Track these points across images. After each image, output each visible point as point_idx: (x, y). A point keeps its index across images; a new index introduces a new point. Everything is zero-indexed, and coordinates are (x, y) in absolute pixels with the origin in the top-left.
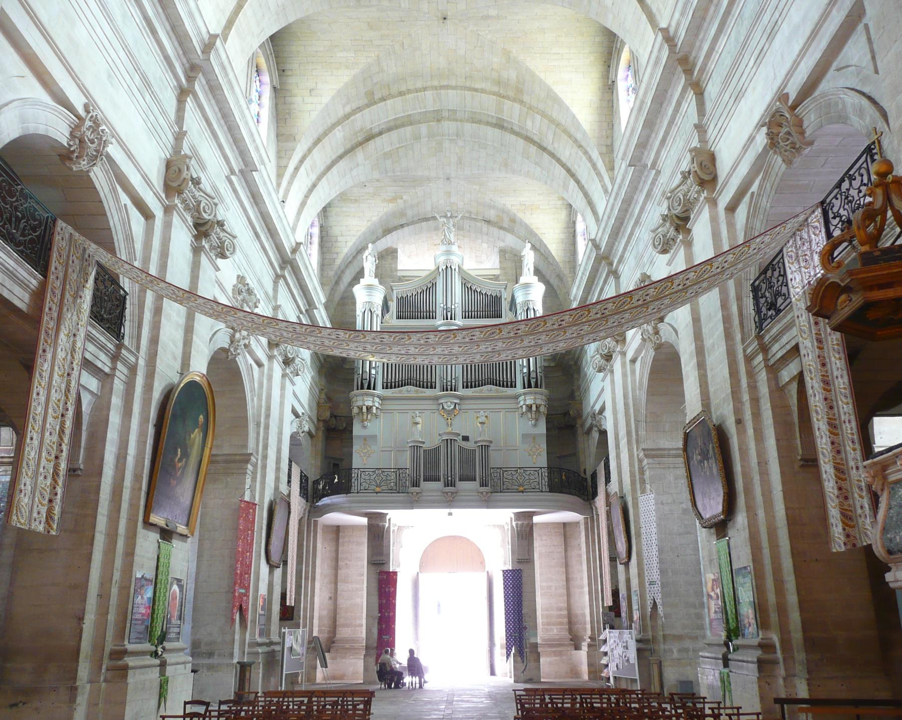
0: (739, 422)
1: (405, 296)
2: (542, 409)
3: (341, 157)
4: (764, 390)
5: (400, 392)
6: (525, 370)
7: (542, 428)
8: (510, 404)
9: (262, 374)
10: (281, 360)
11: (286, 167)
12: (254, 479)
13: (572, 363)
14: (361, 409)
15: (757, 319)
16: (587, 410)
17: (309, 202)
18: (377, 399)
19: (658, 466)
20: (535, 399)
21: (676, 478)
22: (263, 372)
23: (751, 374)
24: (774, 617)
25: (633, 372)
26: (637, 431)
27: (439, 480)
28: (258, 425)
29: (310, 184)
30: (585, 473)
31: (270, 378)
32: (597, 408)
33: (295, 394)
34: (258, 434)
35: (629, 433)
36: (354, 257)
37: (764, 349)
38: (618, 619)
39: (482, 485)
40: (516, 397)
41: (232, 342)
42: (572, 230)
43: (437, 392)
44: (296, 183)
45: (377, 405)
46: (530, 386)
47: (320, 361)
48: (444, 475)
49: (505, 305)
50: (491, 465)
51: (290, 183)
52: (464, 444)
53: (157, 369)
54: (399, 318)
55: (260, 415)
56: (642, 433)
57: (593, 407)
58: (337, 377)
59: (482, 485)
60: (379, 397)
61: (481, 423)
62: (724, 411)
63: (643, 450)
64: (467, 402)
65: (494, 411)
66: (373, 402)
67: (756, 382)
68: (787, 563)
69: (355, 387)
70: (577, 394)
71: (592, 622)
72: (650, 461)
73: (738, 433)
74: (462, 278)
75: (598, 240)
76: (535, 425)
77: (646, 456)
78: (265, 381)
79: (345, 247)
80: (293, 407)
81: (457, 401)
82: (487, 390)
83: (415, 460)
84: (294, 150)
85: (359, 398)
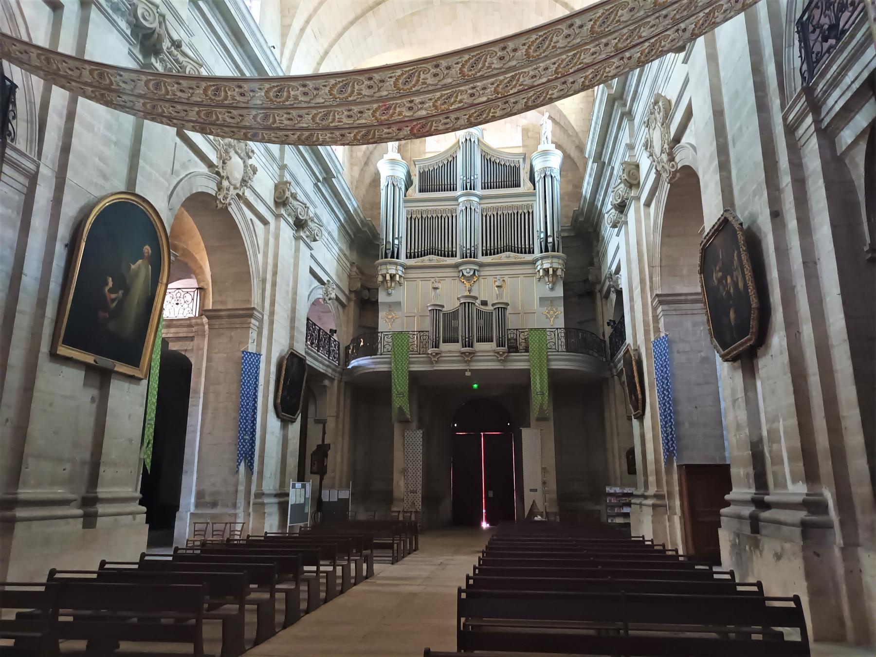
0: (776, 215)
1: (426, 170)
3: (352, 23)
4: (813, 163)
5: (422, 261)
6: (542, 235)
7: (559, 292)
8: (527, 269)
9: (267, 232)
10: (292, 223)
11: (290, 26)
12: (260, 334)
13: (590, 230)
14: (384, 276)
15: (805, 67)
16: (605, 272)
20: (552, 263)
21: (695, 325)
23: (794, 149)
24: (825, 466)
25: (647, 216)
27: (458, 342)
28: (264, 281)
29: (322, 52)
30: (604, 336)
31: (277, 237)
32: (614, 268)
33: (312, 256)
34: (264, 290)
35: (642, 281)
37: (815, 106)
38: (632, 476)
39: (498, 345)
40: (533, 263)
41: (219, 189)
43: (457, 260)
44: (302, 46)
46: (547, 250)
49: (524, 175)
51: (296, 44)
52: (483, 308)
53: (67, 180)
54: (420, 191)
55: (265, 272)
56: (657, 279)
57: (610, 268)
58: (364, 242)
59: (498, 345)
60: (402, 265)
61: (498, 287)
62: (754, 207)
63: (657, 295)
64: (487, 268)
65: (512, 276)
67: (800, 158)
68: (847, 391)
70: (595, 260)
72: (666, 307)
73: (774, 230)
74: (482, 151)
76: (552, 289)
77: (661, 303)
78: (272, 241)
81: (476, 268)
82: (504, 257)
84: (297, 8)
85: (383, 267)
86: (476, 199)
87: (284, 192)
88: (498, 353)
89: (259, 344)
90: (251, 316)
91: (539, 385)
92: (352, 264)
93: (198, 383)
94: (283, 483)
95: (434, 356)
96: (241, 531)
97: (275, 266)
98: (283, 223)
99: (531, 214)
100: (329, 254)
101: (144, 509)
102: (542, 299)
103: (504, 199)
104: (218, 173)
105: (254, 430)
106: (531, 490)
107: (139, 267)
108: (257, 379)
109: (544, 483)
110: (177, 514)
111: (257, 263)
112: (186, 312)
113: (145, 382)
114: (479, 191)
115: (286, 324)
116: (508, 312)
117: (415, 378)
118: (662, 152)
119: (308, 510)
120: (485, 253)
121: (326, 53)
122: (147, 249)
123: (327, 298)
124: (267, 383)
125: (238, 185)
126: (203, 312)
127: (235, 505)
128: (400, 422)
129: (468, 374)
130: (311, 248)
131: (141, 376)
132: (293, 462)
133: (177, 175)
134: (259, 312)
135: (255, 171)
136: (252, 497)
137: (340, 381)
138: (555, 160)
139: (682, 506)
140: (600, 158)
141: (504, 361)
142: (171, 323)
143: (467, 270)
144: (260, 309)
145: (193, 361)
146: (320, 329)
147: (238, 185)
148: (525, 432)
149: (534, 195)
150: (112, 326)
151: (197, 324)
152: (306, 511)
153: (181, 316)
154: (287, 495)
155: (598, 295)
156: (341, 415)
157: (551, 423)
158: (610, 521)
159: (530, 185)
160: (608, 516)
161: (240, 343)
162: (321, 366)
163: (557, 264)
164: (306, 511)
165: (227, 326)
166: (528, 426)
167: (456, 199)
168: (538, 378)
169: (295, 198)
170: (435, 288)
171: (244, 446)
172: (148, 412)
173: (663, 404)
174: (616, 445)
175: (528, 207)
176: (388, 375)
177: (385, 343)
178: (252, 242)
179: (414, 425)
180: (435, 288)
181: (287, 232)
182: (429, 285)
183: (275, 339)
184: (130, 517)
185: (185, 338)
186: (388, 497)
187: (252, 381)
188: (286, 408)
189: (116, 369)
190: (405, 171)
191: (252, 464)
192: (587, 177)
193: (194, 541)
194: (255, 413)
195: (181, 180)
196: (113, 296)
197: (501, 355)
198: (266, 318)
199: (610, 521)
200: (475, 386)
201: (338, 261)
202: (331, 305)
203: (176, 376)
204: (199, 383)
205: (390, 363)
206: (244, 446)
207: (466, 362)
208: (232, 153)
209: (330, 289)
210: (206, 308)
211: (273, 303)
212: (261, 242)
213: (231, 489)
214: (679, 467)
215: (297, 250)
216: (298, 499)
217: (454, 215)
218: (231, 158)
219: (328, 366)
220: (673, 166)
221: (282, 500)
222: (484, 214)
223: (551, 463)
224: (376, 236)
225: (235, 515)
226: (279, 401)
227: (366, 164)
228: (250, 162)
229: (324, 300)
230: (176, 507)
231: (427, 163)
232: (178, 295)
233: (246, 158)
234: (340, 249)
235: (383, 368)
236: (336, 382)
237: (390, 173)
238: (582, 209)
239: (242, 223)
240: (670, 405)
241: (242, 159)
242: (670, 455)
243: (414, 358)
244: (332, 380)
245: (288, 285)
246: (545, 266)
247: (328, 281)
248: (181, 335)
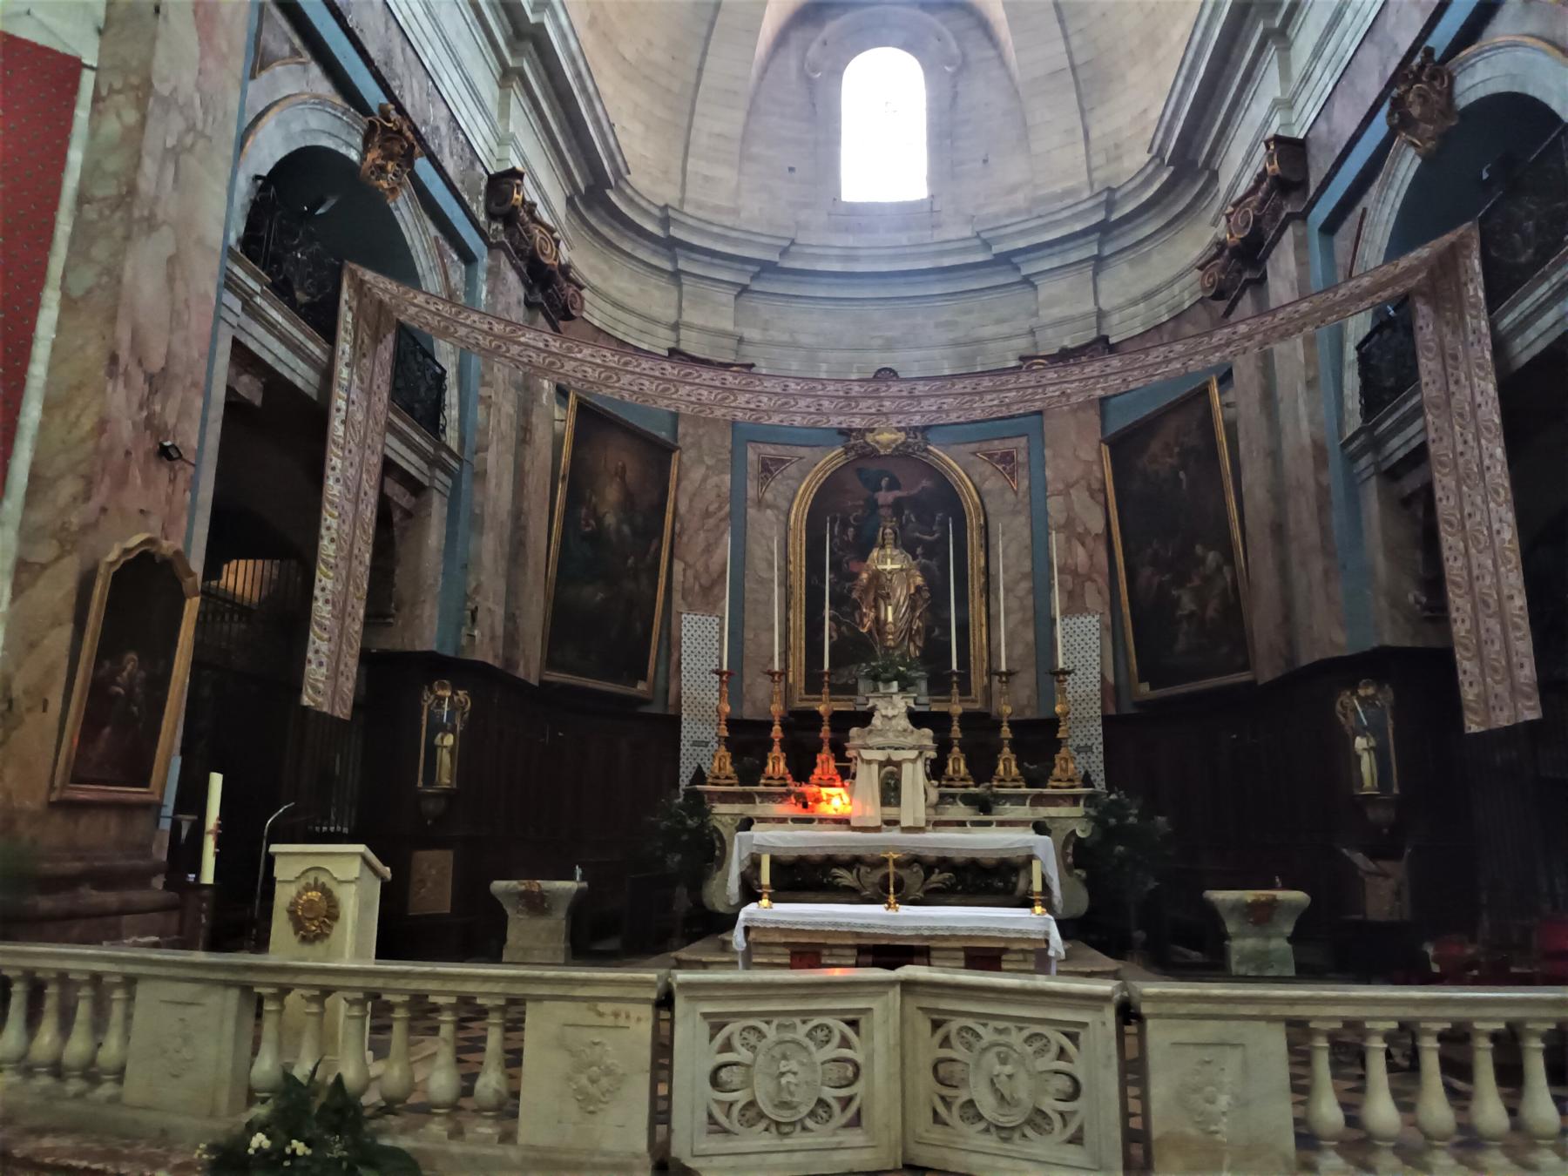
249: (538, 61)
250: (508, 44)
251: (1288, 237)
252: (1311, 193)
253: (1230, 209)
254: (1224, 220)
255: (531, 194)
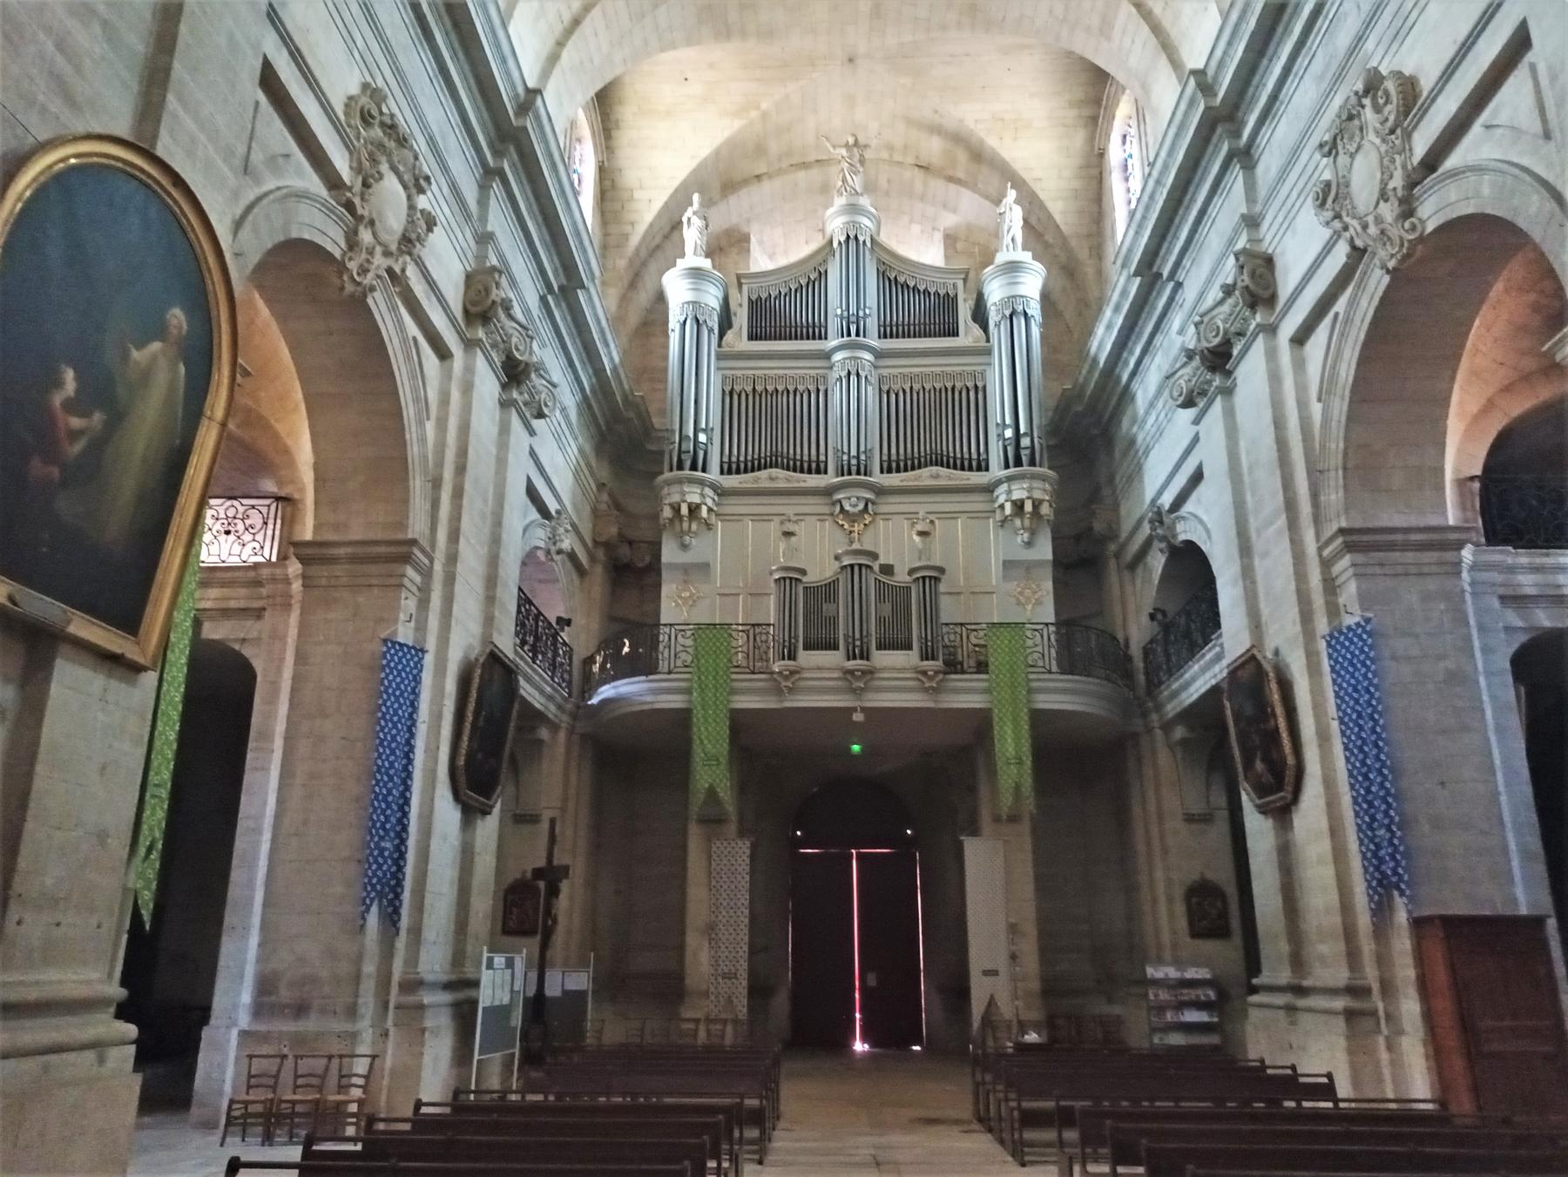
2: (1045, 510)
6: (1009, 433)
8: (976, 503)
9: (447, 376)
12: (424, 603)
14: (676, 509)
17: (565, 54)
18: (708, 491)
19: (1378, 570)
20: (1030, 490)
21: (1426, 597)
22: (451, 369)
25: (1299, 365)
26: (1315, 496)
28: (437, 483)
29: (567, 17)
31: (468, 388)
33: (533, 453)
36: (666, 237)
40: (989, 489)
42: (1095, 172)
45: (710, 502)
46: (1018, 463)
47: (598, 426)
48: (846, 636)
49: (964, 311)
50: (944, 619)
54: (751, 337)
55: (440, 464)
56: (1333, 497)
58: (628, 442)
60: (714, 487)
61: (921, 534)
66: (703, 495)
69: (666, 466)
71: (21, 983)
72: (1360, 558)
74: (879, 261)
75: (1211, 72)
77: (1350, 547)
78: (455, 395)
79: (646, 207)
80: (529, 480)
82: (926, 476)
83: (787, 607)
85: (675, 488)
86: (868, 356)
87: (487, 291)
88: (924, 673)
89: (421, 628)
90: (406, 559)
91: (1012, 745)
92: (601, 486)
93: (270, 716)
94: (458, 958)
95: (786, 678)
96: (367, 1077)
97: (462, 453)
98: (480, 362)
99: (981, 390)
100: (557, 454)
101: (132, 1030)
102: (1008, 565)
103: (927, 363)
104: (349, 206)
105: (405, 829)
106: (986, 973)
107: (154, 358)
108: (414, 707)
109: (1013, 957)
110: (206, 1033)
111: (423, 440)
112: (248, 550)
113: (150, 678)
114: (874, 342)
115: (478, 585)
116: (942, 588)
117: (740, 723)
118: (1383, 196)
119: (517, 1019)
120: (887, 469)
121: (576, 22)
122: (177, 317)
123: (553, 549)
124: (437, 717)
125: (393, 247)
126: (291, 546)
127: (352, 1012)
128: (704, 821)
129: (858, 717)
130: (532, 433)
131: (141, 660)
132: (483, 905)
133: (258, 181)
134: (423, 551)
135: (431, 223)
136: (394, 990)
137: (571, 731)
138: (1032, 283)
139: (1428, 1016)
140: (1151, 265)
141: (936, 691)
142: (216, 576)
143: (851, 500)
144: (425, 543)
145: (258, 665)
146: (540, 613)
147: (393, 247)
148: (974, 849)
149: (989, 352)
150: (66, 506)
151: (274, 580)
152: (513, 1023)
153: (234, 561)
154: (475, 984)
155: (1112, 563)
156: (571, 805)
157: (1025, 827)
158: (1156, 1041)
159: (976, 330)
160: (1154, 1030)
161: (380, 621)
162: (537, 694)
163: (1042, 491)
164: (513, 1023)
165: (344, 580)
166: (975, 832)
167: (827, 356)
168: (1008, 729)
169: (507, 308)
170: (788, 534)
171: (380, 866)
172: (155, 764)
173: (1361, 775)
174: (1159, 874)
175: (973, 375)
176: (682, 719)
177: (675, 647)
178: (415, 390)
179: (732, 828)
180: (788, 534)
181: (487, 384)
182: (774, 527)
183: (457, 627)
184: (90, 1055)
185: (243, 612)
186: (669, 988)
187: (403, 712)
188: (475, 782)
189: (72, 629)
190: (720, 295)
191: (397, 911)
192: (1108, 313)
193: (246, 1103)
194: (408, 788)
195: (266, 194)
196: (76, 422)
197: (931, 678)
198: (438, 567)
199: (1156, 1041)
200: (856, 748)
201: (576, 474)
202: (560, 566)
203: (219, 705)
204: (272, 717)
205: (688, 691)
206: (380, 866)
207: (854, 691)
208: (384, 167)
209: (561, 530)
210: (297, 538)
211: (454, 536)
212: (433, 396)
213: (344, 968)
214: (1419, 924)
215: (504, 429)
216: (498, 992)
217: (822, 388)
218: (381, 177)
219: (550, 698)
220: (1414, 228)
221: (461, 995)
222: (885, 388)
223: (1029, 911)
224: (647, 429)
225: (354, 1036)
226: (461, 762)
227: (633, 285)
228: (422, 202)
229: (548, 552)
230: (203, 1014)
231: (765, 282)
232: (231, 513)
233: (414, 191)
234: (581, 450)
235: (675, 702)
236: (562, 735)
237: (690, 296)
238: (1083, 387)
239: (396, 341)
240: (1385, 777)
241: (405, 187)
242: (1383, 887)
243: (742, 680)
244: (554, 727)
245: (485, 501)
246: (1016, 495)
247: (558, 512)
248: (233, 604)
249: (467, 68)
250: (491, 145)
251: (1259, 345)
252: (1278, 308)
253: (1197, 319)
254: (1192, 329)
255: (506, 291)
